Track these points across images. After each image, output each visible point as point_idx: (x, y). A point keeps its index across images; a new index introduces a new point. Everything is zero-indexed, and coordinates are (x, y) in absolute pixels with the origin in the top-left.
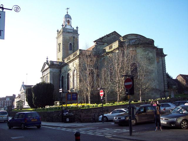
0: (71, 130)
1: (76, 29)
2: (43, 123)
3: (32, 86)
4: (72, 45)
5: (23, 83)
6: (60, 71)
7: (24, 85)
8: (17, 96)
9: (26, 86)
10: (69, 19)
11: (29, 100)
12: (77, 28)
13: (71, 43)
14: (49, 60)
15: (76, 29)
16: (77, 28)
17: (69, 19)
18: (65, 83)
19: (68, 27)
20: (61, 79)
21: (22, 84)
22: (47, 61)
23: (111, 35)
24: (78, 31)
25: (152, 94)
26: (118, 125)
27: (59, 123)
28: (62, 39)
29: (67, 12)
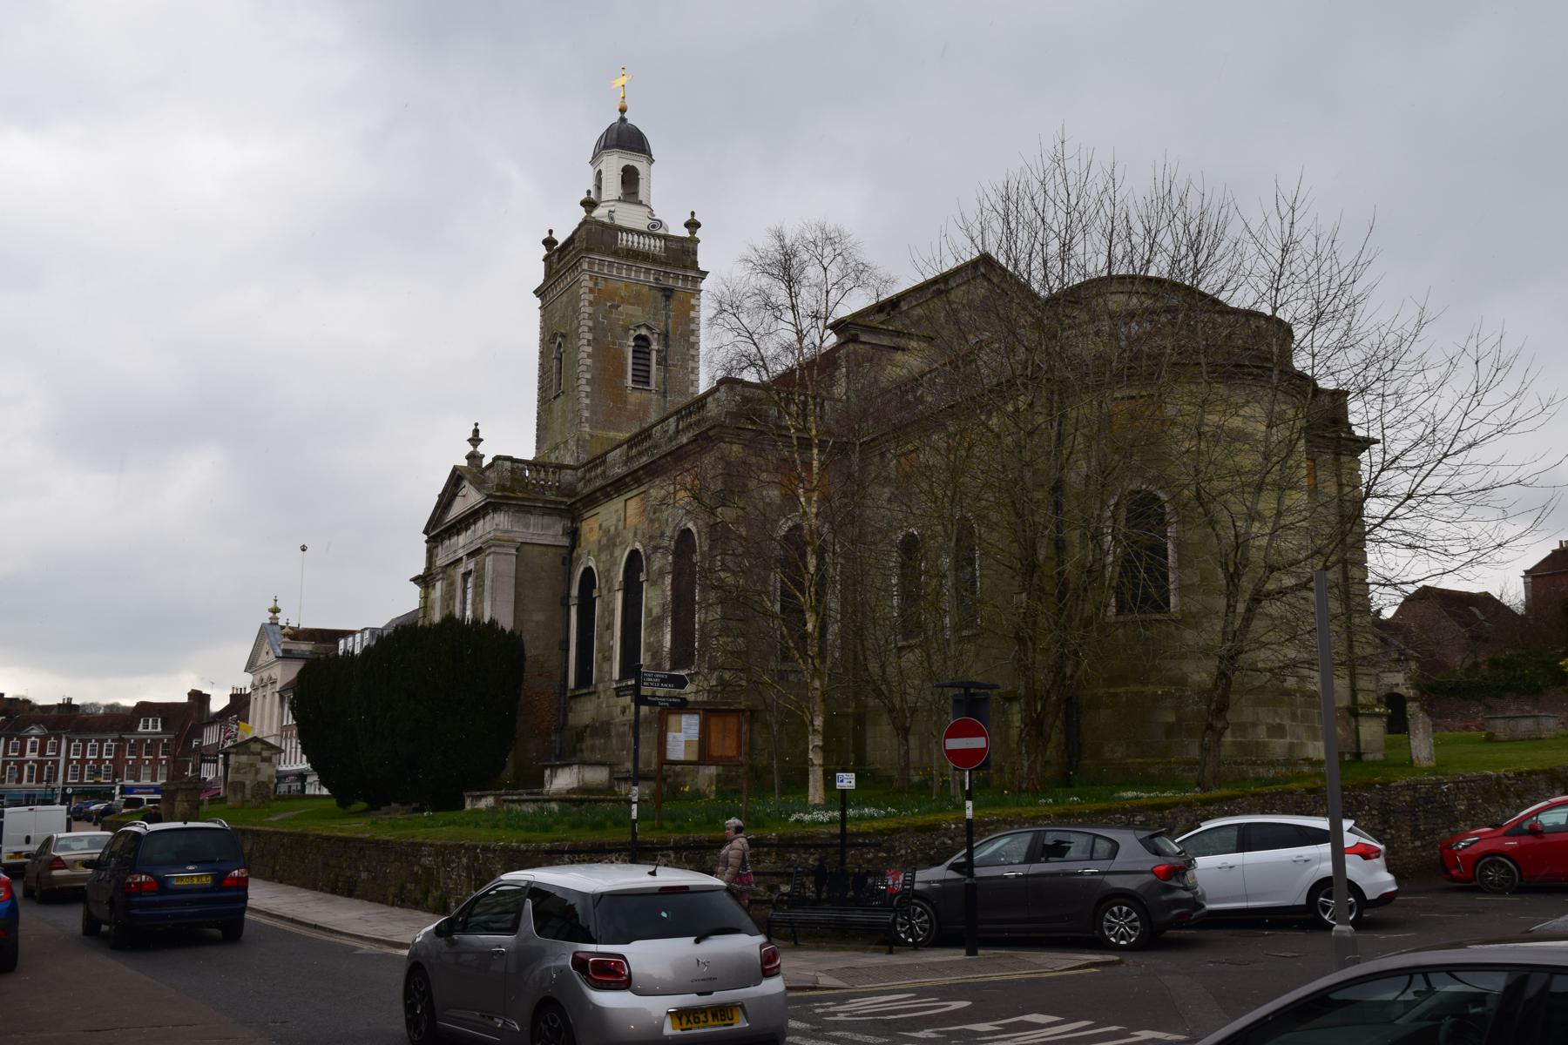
0: (829, 1006)
1: (685, 233)
2: (263, 896)
3: (345, 634)
4: (655, 346)
5: (275, 611)
6: (574, 534)
7: (282, 622)
8: (218, 703)
9: (298, 635)
10: (639, 164)
11: (311, 732)
12: (693, 225)
13: (644, 332)
14: (488, 452)
15: (685, 233)
16: (693, 225)
17: (639, 164)
18: (610, 627)
19: (629, 216)
20: (575, 592)
21: (266, 618)
22: (474, 458)
23: (952, 283)
24: (700, 247)
25: (1277, 731)
26: (1333, 996)
27: (306, 895)
28: (702, 338)
29: (623, 110)
